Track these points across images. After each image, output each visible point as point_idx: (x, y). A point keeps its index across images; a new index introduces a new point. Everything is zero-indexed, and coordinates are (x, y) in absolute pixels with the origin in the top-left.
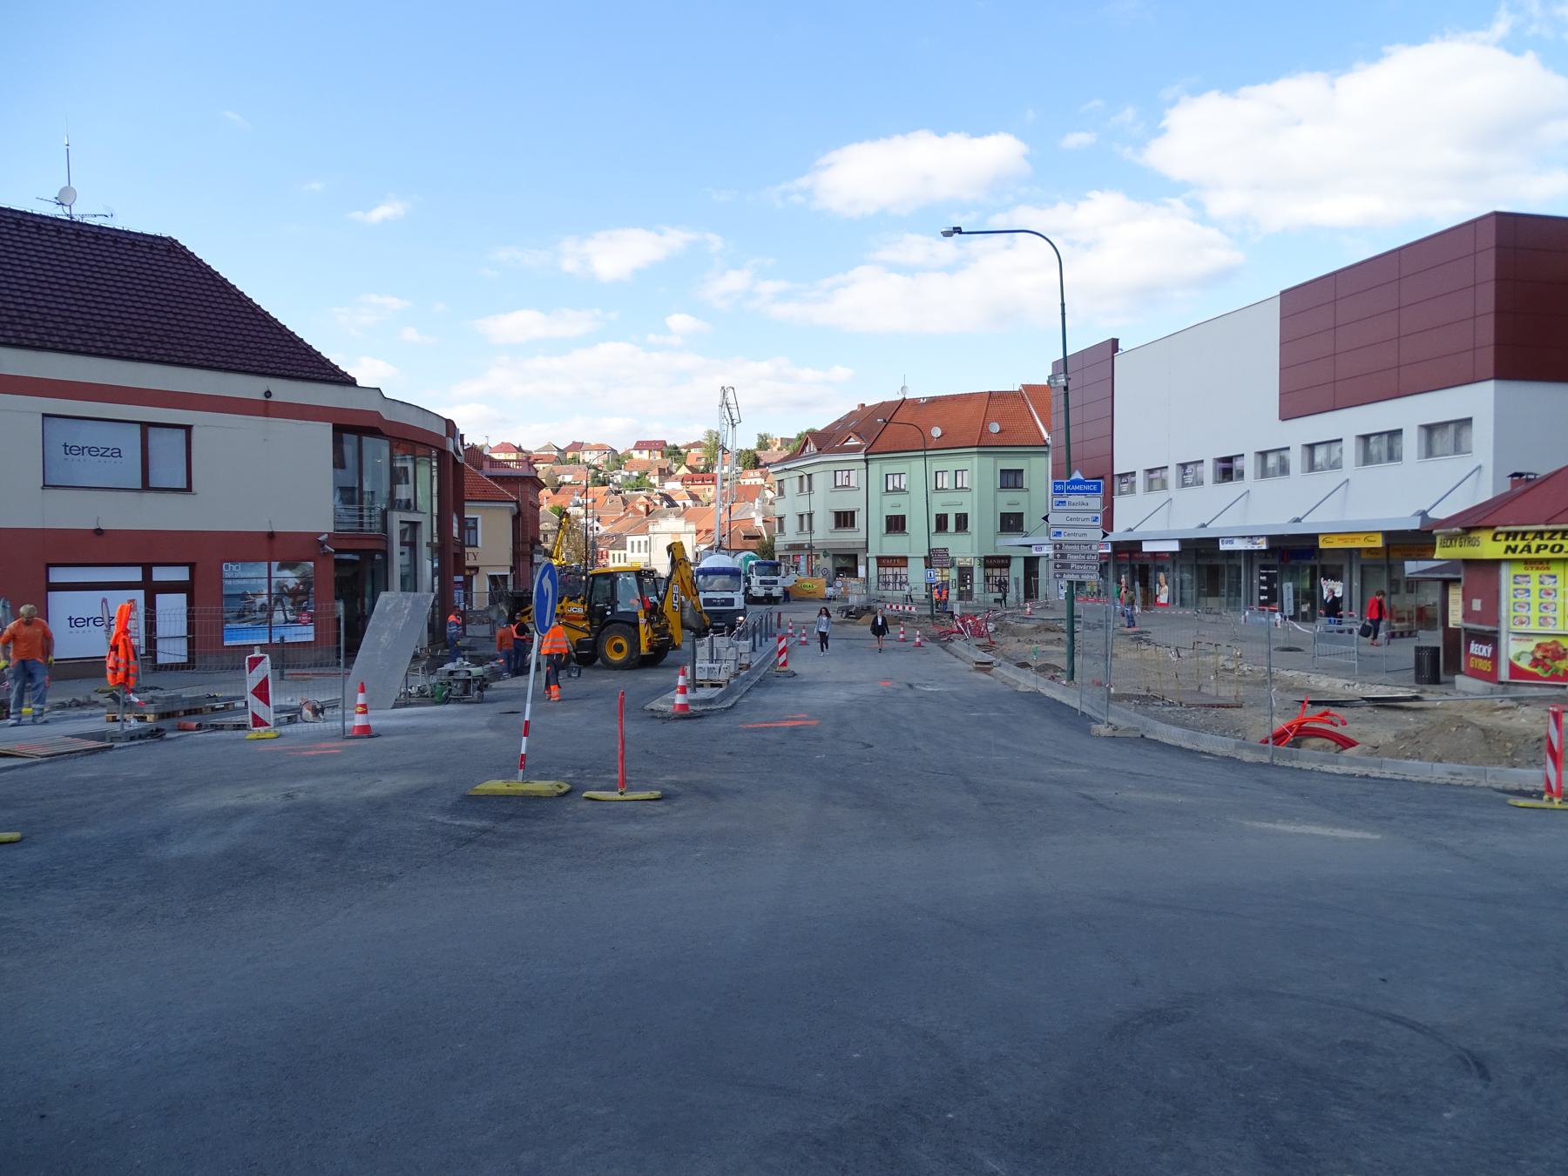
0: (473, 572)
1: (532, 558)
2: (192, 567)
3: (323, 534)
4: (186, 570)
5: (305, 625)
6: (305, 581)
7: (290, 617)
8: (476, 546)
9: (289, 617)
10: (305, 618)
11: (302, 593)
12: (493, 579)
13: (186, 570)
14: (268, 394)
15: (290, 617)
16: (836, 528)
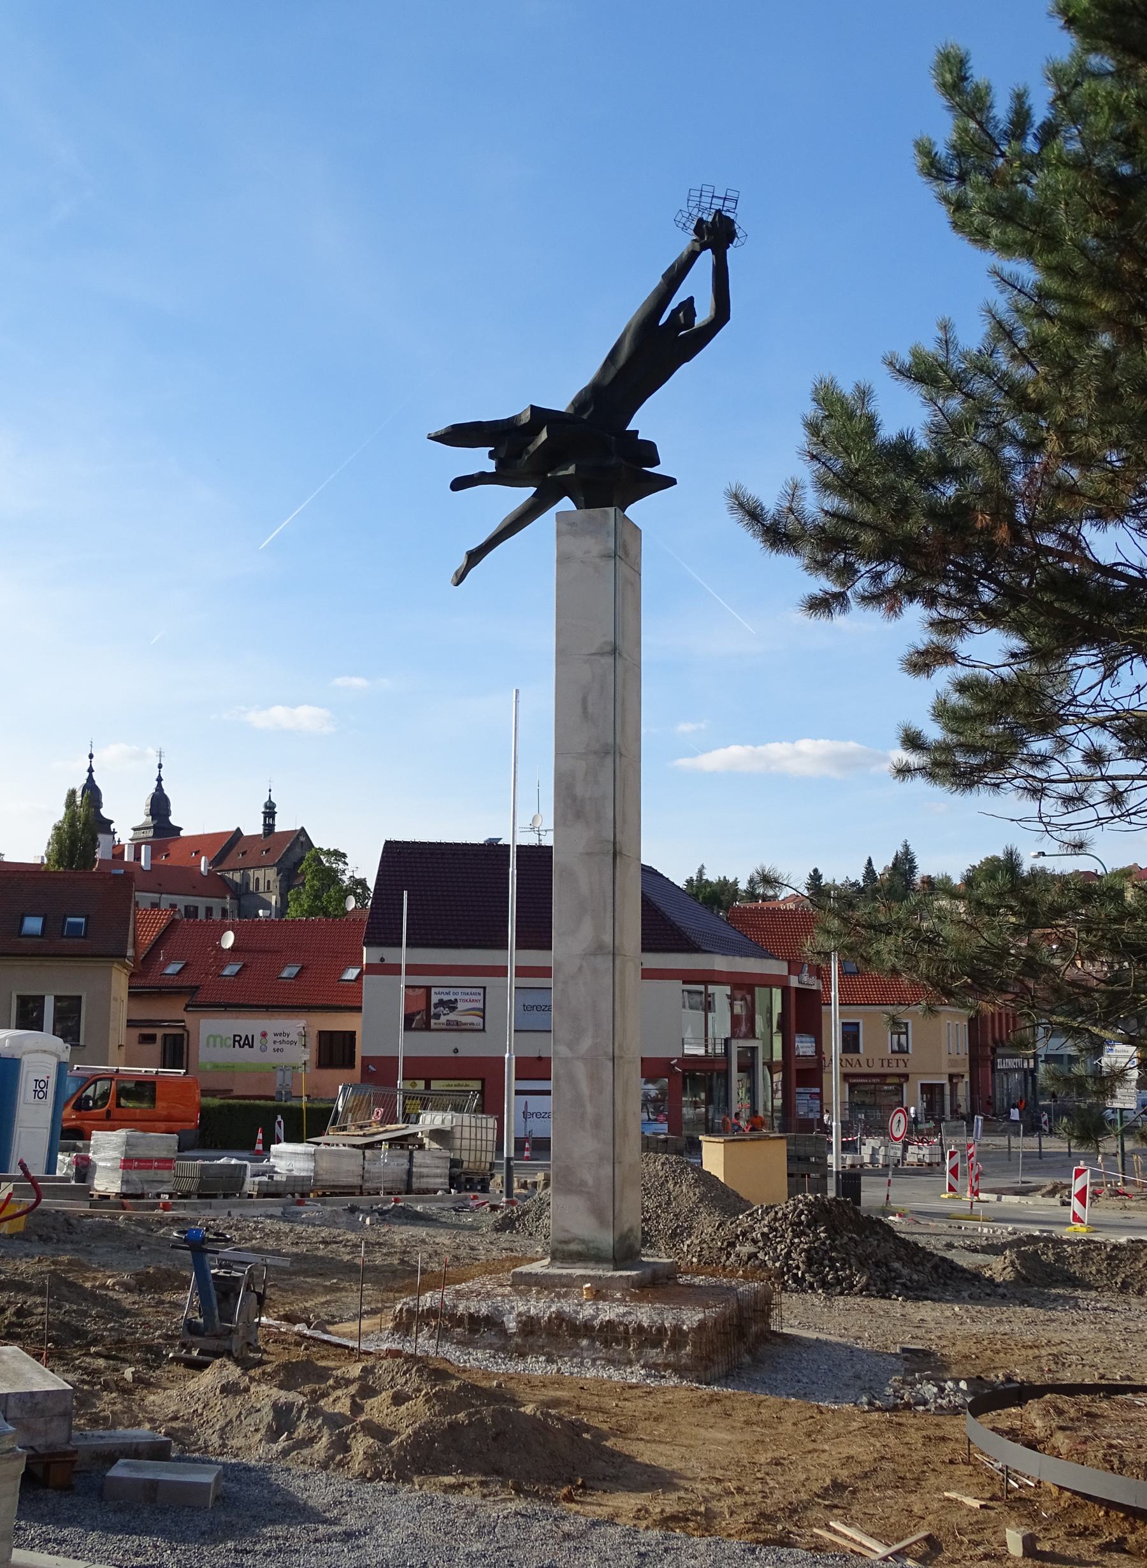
0: (902, 1080)
1: (994, 1064)
2: (483, 1080)
3: (674, 1059)
4: (479, 1082)
5: (661, 1123)
6: (662, 1091)
7: (652, 1117)
8: (907, 1052)
9: (651, 1117)
10: (661, 1118)
11: (660, 1100)
12: (927, 1089)
13: (479, 1082)
14: (382, 960)
15: (652, 1117)
16: (44, 997)
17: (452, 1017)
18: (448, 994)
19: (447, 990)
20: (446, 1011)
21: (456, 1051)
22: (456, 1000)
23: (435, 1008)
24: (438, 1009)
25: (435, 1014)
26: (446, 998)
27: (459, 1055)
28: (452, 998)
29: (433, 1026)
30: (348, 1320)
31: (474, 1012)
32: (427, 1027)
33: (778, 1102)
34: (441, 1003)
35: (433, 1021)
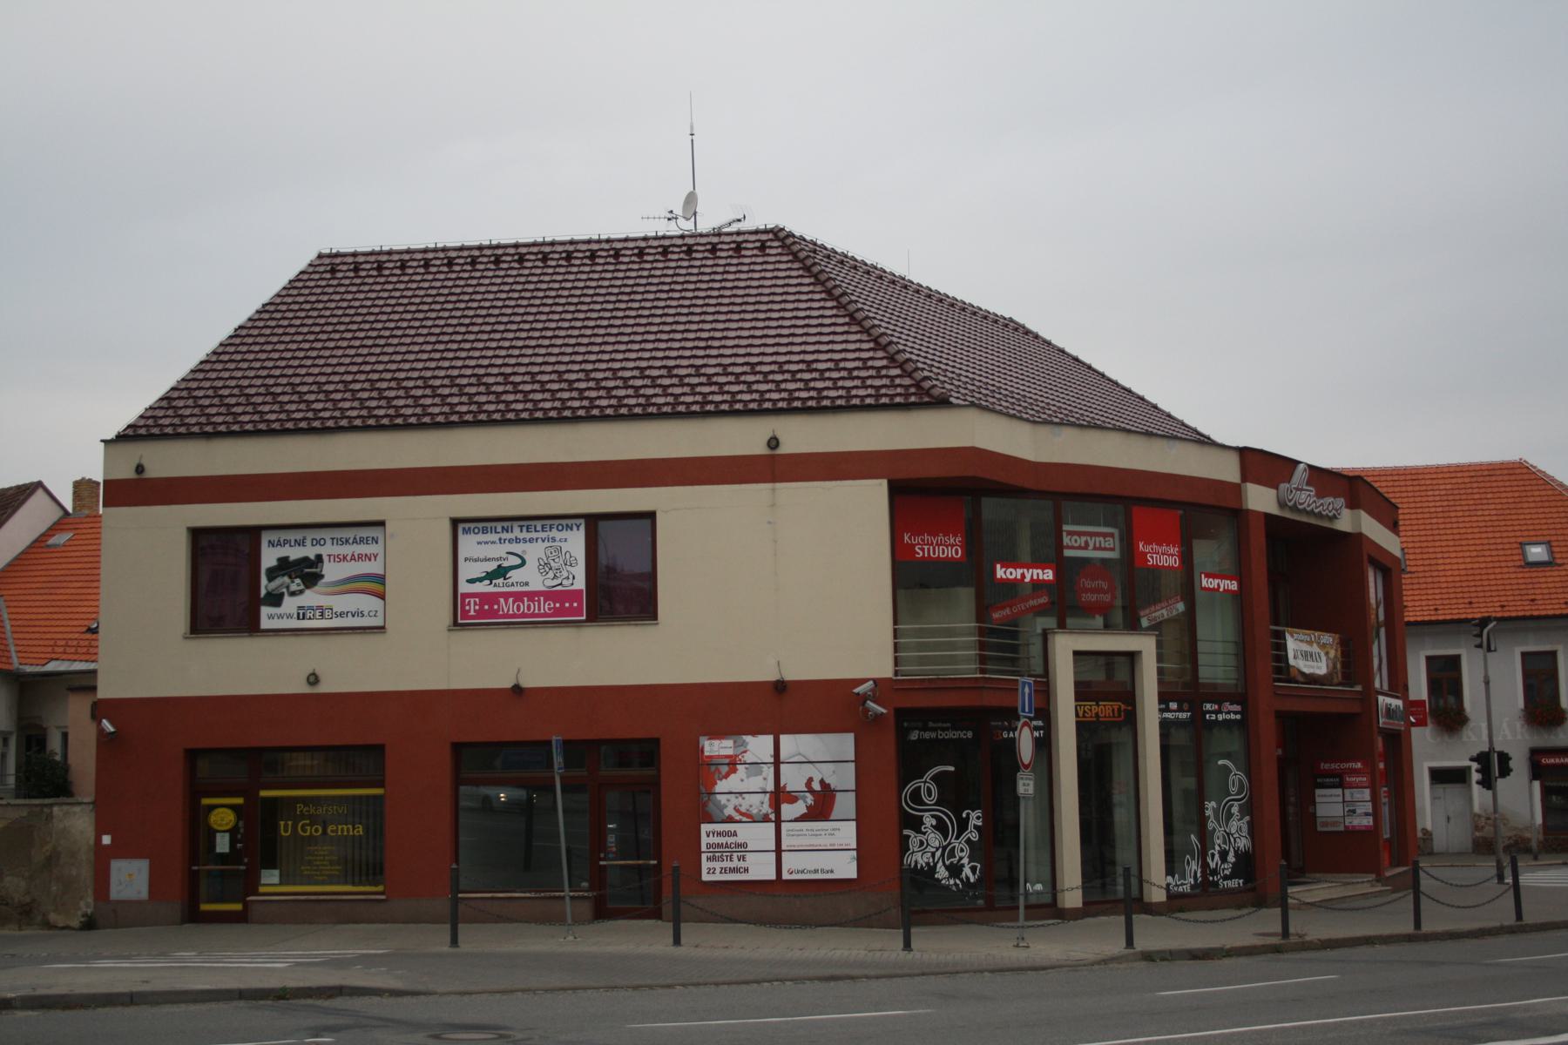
13: (1531, 559)
14: (140, 469)
17: (311, 598)
18: (301, 543)
19: (298, 535)
20: (296, 585)
21: (313, 679)
22: (319, 558)
23: (270, 579)
24: (278, 581)
25: (269, 594)
26: (295, 553)
27: (323, 688)
28: (310, 552)
29: (265, 623)
30: (1360, 815)
31: (348, 586)
32: (304, 618)
33: (1211, 805)
34: (284, 566)
35: (265, 611)
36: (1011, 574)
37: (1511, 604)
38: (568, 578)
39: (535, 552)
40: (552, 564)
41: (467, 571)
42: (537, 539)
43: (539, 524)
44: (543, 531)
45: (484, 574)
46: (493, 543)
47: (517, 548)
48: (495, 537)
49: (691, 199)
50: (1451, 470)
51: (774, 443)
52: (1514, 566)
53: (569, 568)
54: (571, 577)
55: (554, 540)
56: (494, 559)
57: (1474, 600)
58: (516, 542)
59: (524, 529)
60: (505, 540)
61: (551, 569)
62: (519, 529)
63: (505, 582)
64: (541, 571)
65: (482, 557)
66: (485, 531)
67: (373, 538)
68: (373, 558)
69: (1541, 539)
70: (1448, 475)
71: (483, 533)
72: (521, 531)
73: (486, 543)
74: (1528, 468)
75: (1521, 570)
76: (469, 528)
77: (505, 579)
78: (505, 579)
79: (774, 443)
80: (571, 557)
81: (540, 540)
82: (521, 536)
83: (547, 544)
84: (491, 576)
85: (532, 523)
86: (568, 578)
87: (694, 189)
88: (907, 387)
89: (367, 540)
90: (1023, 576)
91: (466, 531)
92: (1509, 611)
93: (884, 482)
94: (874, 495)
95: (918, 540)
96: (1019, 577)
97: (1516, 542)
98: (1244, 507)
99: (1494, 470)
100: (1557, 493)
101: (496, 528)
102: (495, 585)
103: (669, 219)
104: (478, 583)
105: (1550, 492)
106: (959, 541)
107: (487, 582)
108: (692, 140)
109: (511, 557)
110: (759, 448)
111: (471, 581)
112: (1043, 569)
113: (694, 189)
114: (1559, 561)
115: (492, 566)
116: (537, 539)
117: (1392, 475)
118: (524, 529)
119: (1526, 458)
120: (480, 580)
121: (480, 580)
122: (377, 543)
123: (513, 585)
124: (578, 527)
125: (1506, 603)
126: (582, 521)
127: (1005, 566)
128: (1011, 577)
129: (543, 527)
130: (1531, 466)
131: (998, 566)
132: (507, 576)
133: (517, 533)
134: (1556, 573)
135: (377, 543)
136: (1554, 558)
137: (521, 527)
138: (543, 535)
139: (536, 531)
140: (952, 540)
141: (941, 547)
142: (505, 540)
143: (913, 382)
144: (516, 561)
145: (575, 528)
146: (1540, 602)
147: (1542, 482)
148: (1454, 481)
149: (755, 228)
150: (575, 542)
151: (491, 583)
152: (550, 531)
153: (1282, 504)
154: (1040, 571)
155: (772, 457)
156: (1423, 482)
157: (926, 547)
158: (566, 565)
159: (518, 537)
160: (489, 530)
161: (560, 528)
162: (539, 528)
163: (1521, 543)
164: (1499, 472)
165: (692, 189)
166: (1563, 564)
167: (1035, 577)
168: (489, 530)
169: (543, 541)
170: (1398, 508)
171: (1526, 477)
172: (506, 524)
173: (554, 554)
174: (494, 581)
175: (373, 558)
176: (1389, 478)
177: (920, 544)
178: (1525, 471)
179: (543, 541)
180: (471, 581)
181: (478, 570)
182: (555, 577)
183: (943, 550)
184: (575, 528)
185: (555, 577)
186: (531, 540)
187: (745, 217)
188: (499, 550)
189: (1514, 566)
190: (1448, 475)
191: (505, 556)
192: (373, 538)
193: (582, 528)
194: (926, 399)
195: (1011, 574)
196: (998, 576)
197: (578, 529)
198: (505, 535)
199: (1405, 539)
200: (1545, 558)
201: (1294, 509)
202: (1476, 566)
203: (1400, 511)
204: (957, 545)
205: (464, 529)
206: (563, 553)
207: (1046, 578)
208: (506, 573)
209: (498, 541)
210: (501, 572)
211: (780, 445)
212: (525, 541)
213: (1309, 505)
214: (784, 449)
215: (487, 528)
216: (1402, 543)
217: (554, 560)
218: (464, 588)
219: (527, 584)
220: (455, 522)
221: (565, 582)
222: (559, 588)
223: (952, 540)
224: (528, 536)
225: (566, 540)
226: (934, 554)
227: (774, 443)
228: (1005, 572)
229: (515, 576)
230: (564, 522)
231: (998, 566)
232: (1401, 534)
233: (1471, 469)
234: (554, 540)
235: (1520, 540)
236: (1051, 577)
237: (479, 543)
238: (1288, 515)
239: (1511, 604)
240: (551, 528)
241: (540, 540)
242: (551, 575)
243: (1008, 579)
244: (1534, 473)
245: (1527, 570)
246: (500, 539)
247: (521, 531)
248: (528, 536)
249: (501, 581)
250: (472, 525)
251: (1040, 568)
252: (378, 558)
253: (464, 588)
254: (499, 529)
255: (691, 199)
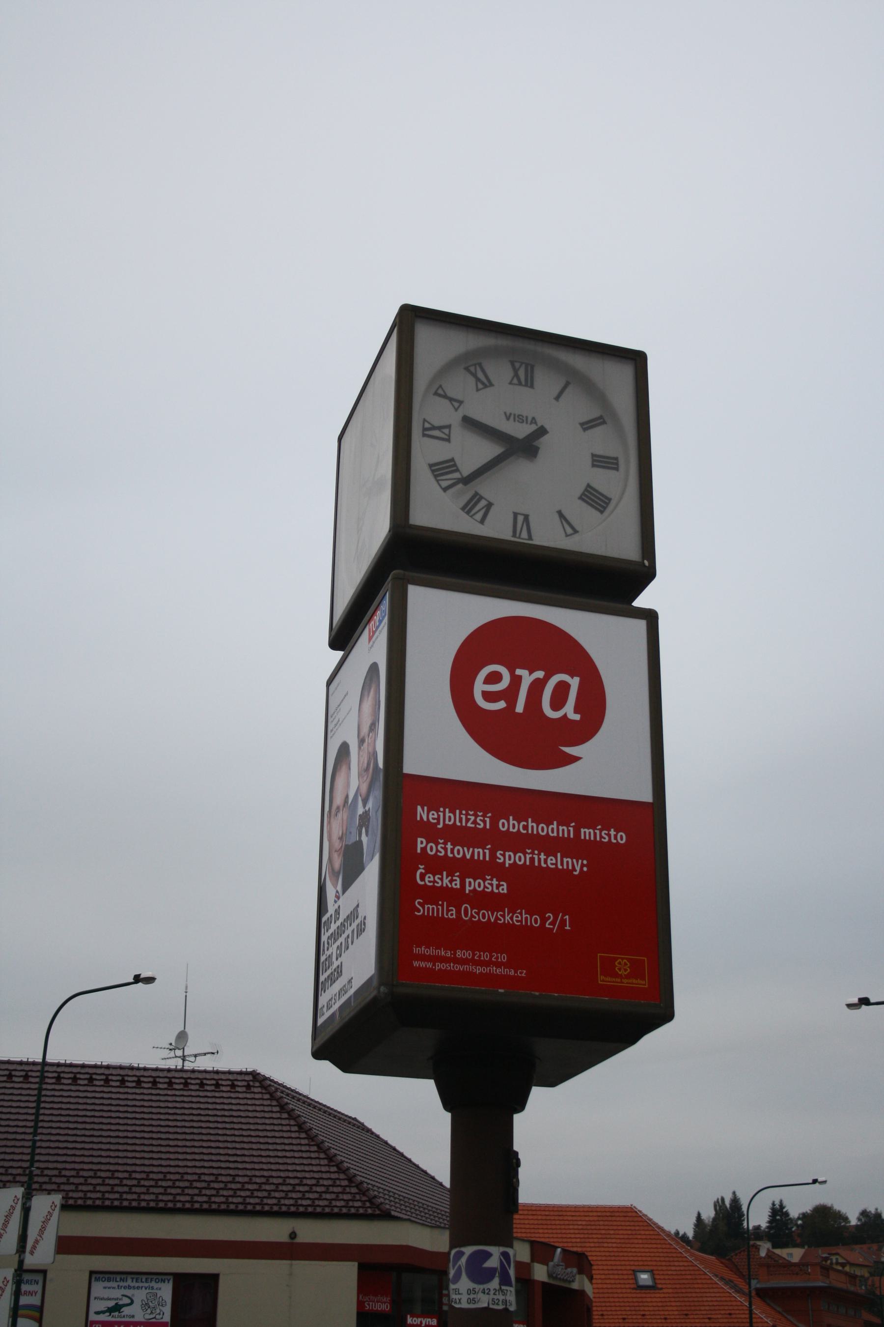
13: (641, 1283)
36: (415, 1321)
37: (630, 1317)
38: (159, 1314)
39: (140, 1296)
40: (151, 1304)
41: (96, 1306)
42: (142, 1287)
43: (144, 1278)
44: (146, 1282)
45: (107, 1309)
46: (114, 1288)
47: (129, 1292)
48: (115, 1284)
49: (182, 1037)
50: (585, 1210)
51: (293, 1235)
52: (630, 1288)
53: (161, 1307)
54: (162, 1313)
55: (152, 1288)
56: (113, 1299)
57: (605, 1313)
58: (129, 1288)
59: (134, 1280)
60: (121, 1287)
61: (149, 1307)
62: (131, 1280)
63: (120, 1314)
64: (143, 1308)
65: (106, 1297)
66: (109, 1280)
67: (35, 1281)
68: (34, 1294)
69: (647, 1268)
70: (582, 1214)
71: (108, 1281)
72: (132, 1281)
73: (109, 1288)
74: (636, 1212)
75: (634, 1291)
76: (99, 1278)
77: (119, 1313)
78: (119, 1313)
79: (293, 1235)
80: (162, 1300)
81: (143, 1288)
82: (132, 1284)
83: (148, 1291)
84: (110, 1310)
85: (140, 1276)
86: (159, 1314)
87: (185, 1029)
88: (364, 1202)
89: (31, 1282)
90: (421, 1322)
91: (97, 1280)
92: (628, 1323)
93: (356, 1264)
94: (349, 1271)
95: (367, 1298)
96: (419, 1323)
97: (630, 1270)
98: (532, 1278)
99: (613, 1212)
100: (656, 1233)
101: (116, 1279)
102: (113, 1316)
103: (170, 1050)
104: (101, 1314)
105: (651, 1233)
106: (389, 1300)
107: (108, 1314)
108: (186, 996)
109: (124, 1298)
110: (284, 1238)
111: (97, 1313)
112: (432, 1319)
113: (185, 1029)
114: (660, 1286)
115: (111, 1304)
116: (142, 1287)
117: (544, 1211)
118: (134, 1280)
119: (635, 1204)
120: (103, 1312)
121: (103, 1312)
122: (37, 1284)
123: (124, 1316)
124: (169, 1281)
125: (626, 1317)
126: (171, 1278)
127: (412, 1316)
128: (415, 1323)
129: (146, 1279)
130: (639, 1211)
131: (409, 1316)
132: (121, 1311)
133: (129, 1282)
134: (658, 1295)
135: (37, 1284)
136: (656, 1283)
137: (133, 1279)
138: (146, 1285)
139: (142, 1282)
140: (385, 1299)
141: (379, 1304)
142: (121, 1287)
143: (367, 1199)
144: (128, 1301)
145: (166, 1281)
146: (648, 1317)
147: (646, 1224)
148: (587, 1218)
149: (239, 1070)
150: (166, 1291)
151: (110, 1315)
152: (151, 1282)
153: (550, 1275)
154: (430, 1320)
155: (292, 1244)
156: (566, 1218)
157: (371, 1303)
158: (159, 1305)
159: (130, 1285)
160: (112, 1279)
161: (157, 1280)
162: (144, 1280)
163: (633, 1270)
164: (617, 1214)
165: (183, 1029)
166: (662, 1289)
167: (427, 1323)
168: (112, 1279)
169: (146, 1289)
170: (592, 1265)
171: (674, 1255)
172: (123, 1276)
173: (152, 1298)
174: (112, 1314)
175: (34, 1294)
176: (544, 1213)
177: (368, 1301)
178: (634, 1214)
179: (146, 1289)
180: (97, 1313)
181: (103, 1305)
182: (152, 1313)
183: (380, 1305)
184: (166, 1281)
185: (152, 1313)
186: (138, 1288)
187: (218, 1052)
188: (117, 1293)
189: (630, 1288)
190: (582, 1214)
191: (121, 1297)
192: (35, 1281)
193: (171, 1282)
194: (378, 1212)
195: (415, 1321)
196: (408, 1323)
197: (168, 1282)
198: (121, 1284)
199: (595, 1286)
200: (650, 1283)
201: (556, 1278)
202: (605, 1286)
203: (595, 1267)
204: (387, 1302)
205: (96, 1278)
206: (158, 1298)
207: (433, 1324)
208: (121, 1308)
209: (117, 1287)
210: (117, 1308)
211: (297, 1237)
212: (134, 1288)
213: (562, 1275)
214: (299, 1240)
215: (111, 1278)
216: (594, 1288)
217: (151, 1301)
218: (93, 1317)
219: (133, 1316)
220: (92, 1273)
221: (158, 1317)
222: (154, 1320)
223: (385, 1299)
224: (137, 1285)
225: (160, 1289)
226: (375, 1307)
227: (293, 1236)
228: (412, 1320)
229: (126, 1311)
230: (160, 1277)
231: (409, 1316)
232: (594, 1281)
233: (598, 1210)
234: (152, 1288)
235: (633, 1268)
236: (435, 1324)
237: (105, 1288)
238: (552, 1282)
239: (630, 1317)
240: (151, 1281)
241: (143, 1288)
242: (149, 1311)
243: (413, 1325)
244: (640, 1216)
245: (638, 1291)
246: (118, 1286)
247: (132, 1281)
248: (137, 1285)
249: (117, 1314)
250: (101, 1276)
251: (430, 1318)
252: (37, 1294)
253: (93, 1317)
254: (118, 1280)
255: (182, 1037)
